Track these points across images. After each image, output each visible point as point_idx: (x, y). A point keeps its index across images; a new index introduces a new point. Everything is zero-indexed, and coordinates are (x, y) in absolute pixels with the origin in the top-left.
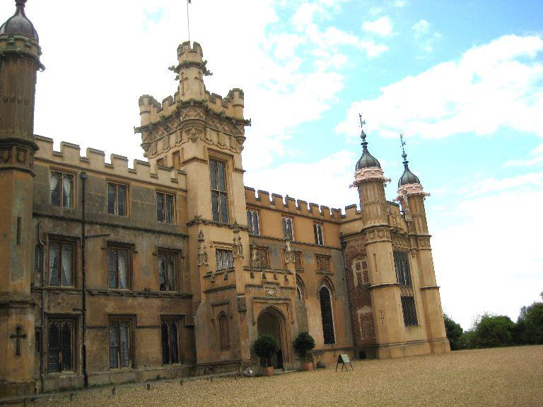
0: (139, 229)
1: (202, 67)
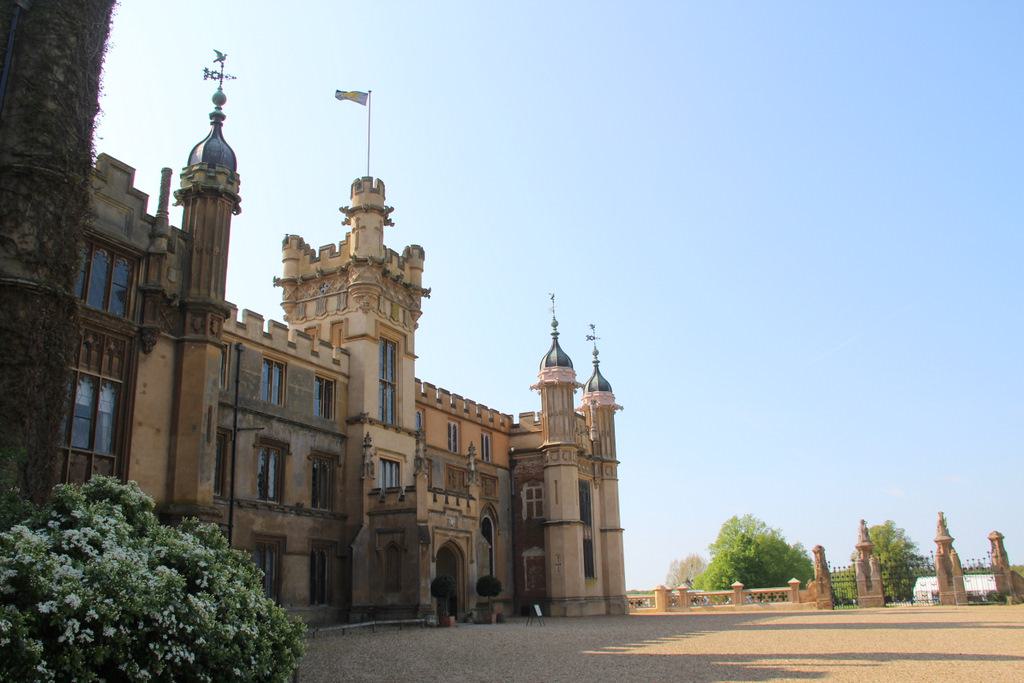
0: (292, 423)
1: (384, 214)
